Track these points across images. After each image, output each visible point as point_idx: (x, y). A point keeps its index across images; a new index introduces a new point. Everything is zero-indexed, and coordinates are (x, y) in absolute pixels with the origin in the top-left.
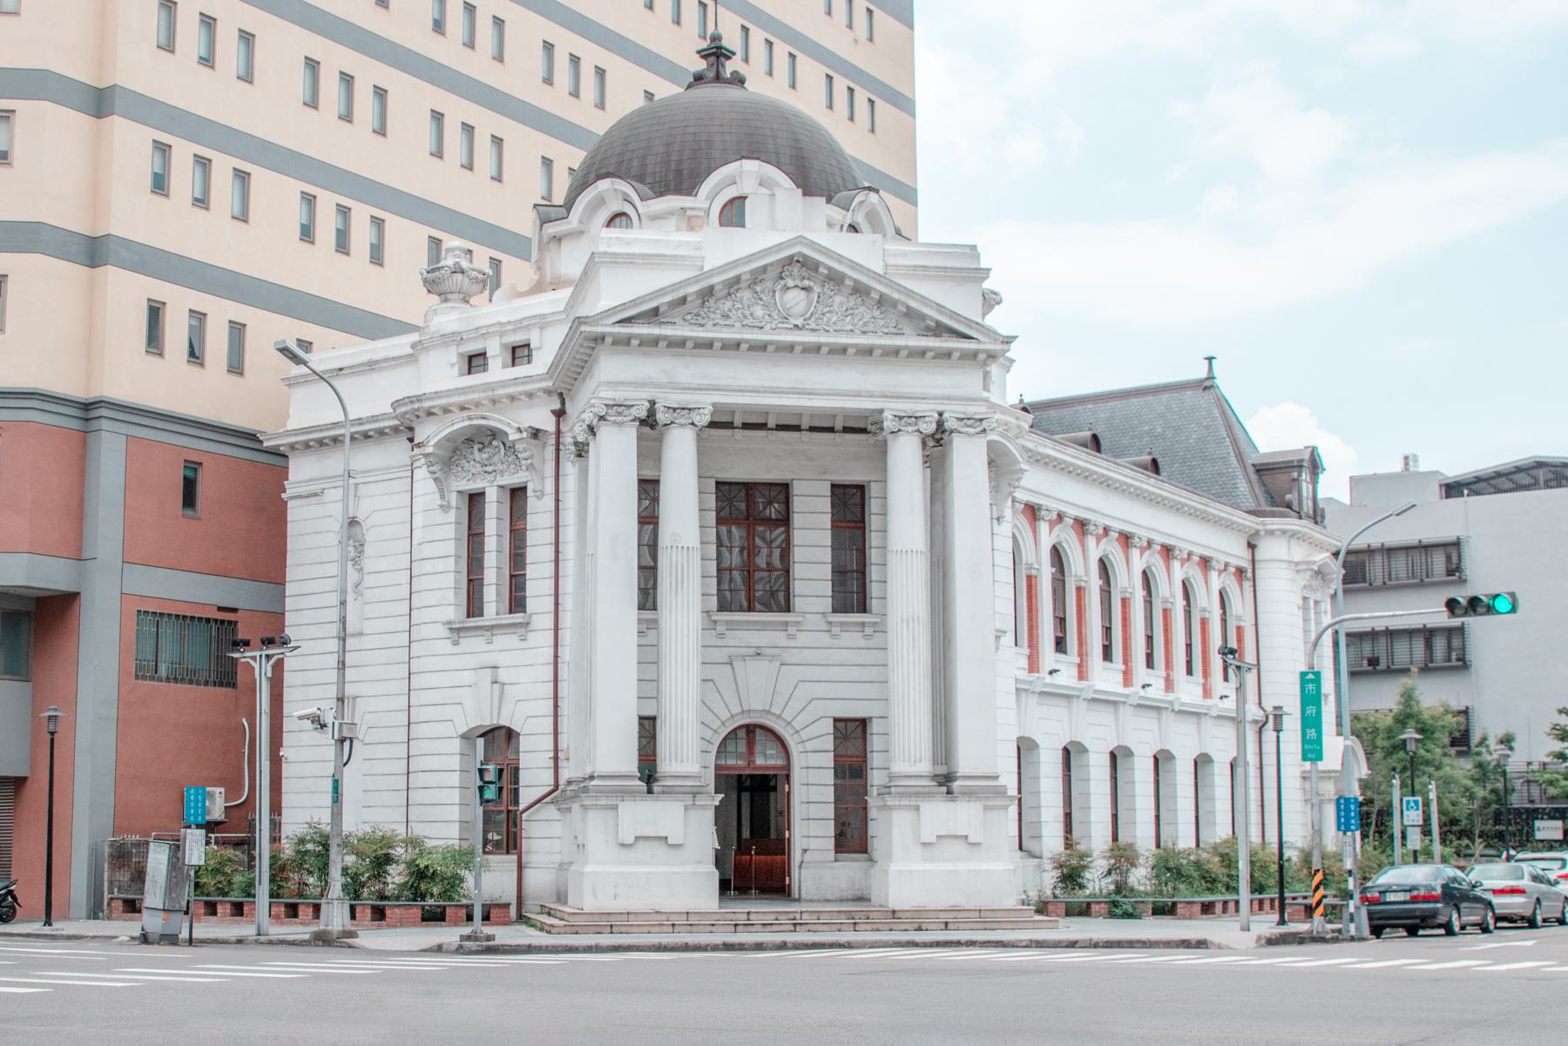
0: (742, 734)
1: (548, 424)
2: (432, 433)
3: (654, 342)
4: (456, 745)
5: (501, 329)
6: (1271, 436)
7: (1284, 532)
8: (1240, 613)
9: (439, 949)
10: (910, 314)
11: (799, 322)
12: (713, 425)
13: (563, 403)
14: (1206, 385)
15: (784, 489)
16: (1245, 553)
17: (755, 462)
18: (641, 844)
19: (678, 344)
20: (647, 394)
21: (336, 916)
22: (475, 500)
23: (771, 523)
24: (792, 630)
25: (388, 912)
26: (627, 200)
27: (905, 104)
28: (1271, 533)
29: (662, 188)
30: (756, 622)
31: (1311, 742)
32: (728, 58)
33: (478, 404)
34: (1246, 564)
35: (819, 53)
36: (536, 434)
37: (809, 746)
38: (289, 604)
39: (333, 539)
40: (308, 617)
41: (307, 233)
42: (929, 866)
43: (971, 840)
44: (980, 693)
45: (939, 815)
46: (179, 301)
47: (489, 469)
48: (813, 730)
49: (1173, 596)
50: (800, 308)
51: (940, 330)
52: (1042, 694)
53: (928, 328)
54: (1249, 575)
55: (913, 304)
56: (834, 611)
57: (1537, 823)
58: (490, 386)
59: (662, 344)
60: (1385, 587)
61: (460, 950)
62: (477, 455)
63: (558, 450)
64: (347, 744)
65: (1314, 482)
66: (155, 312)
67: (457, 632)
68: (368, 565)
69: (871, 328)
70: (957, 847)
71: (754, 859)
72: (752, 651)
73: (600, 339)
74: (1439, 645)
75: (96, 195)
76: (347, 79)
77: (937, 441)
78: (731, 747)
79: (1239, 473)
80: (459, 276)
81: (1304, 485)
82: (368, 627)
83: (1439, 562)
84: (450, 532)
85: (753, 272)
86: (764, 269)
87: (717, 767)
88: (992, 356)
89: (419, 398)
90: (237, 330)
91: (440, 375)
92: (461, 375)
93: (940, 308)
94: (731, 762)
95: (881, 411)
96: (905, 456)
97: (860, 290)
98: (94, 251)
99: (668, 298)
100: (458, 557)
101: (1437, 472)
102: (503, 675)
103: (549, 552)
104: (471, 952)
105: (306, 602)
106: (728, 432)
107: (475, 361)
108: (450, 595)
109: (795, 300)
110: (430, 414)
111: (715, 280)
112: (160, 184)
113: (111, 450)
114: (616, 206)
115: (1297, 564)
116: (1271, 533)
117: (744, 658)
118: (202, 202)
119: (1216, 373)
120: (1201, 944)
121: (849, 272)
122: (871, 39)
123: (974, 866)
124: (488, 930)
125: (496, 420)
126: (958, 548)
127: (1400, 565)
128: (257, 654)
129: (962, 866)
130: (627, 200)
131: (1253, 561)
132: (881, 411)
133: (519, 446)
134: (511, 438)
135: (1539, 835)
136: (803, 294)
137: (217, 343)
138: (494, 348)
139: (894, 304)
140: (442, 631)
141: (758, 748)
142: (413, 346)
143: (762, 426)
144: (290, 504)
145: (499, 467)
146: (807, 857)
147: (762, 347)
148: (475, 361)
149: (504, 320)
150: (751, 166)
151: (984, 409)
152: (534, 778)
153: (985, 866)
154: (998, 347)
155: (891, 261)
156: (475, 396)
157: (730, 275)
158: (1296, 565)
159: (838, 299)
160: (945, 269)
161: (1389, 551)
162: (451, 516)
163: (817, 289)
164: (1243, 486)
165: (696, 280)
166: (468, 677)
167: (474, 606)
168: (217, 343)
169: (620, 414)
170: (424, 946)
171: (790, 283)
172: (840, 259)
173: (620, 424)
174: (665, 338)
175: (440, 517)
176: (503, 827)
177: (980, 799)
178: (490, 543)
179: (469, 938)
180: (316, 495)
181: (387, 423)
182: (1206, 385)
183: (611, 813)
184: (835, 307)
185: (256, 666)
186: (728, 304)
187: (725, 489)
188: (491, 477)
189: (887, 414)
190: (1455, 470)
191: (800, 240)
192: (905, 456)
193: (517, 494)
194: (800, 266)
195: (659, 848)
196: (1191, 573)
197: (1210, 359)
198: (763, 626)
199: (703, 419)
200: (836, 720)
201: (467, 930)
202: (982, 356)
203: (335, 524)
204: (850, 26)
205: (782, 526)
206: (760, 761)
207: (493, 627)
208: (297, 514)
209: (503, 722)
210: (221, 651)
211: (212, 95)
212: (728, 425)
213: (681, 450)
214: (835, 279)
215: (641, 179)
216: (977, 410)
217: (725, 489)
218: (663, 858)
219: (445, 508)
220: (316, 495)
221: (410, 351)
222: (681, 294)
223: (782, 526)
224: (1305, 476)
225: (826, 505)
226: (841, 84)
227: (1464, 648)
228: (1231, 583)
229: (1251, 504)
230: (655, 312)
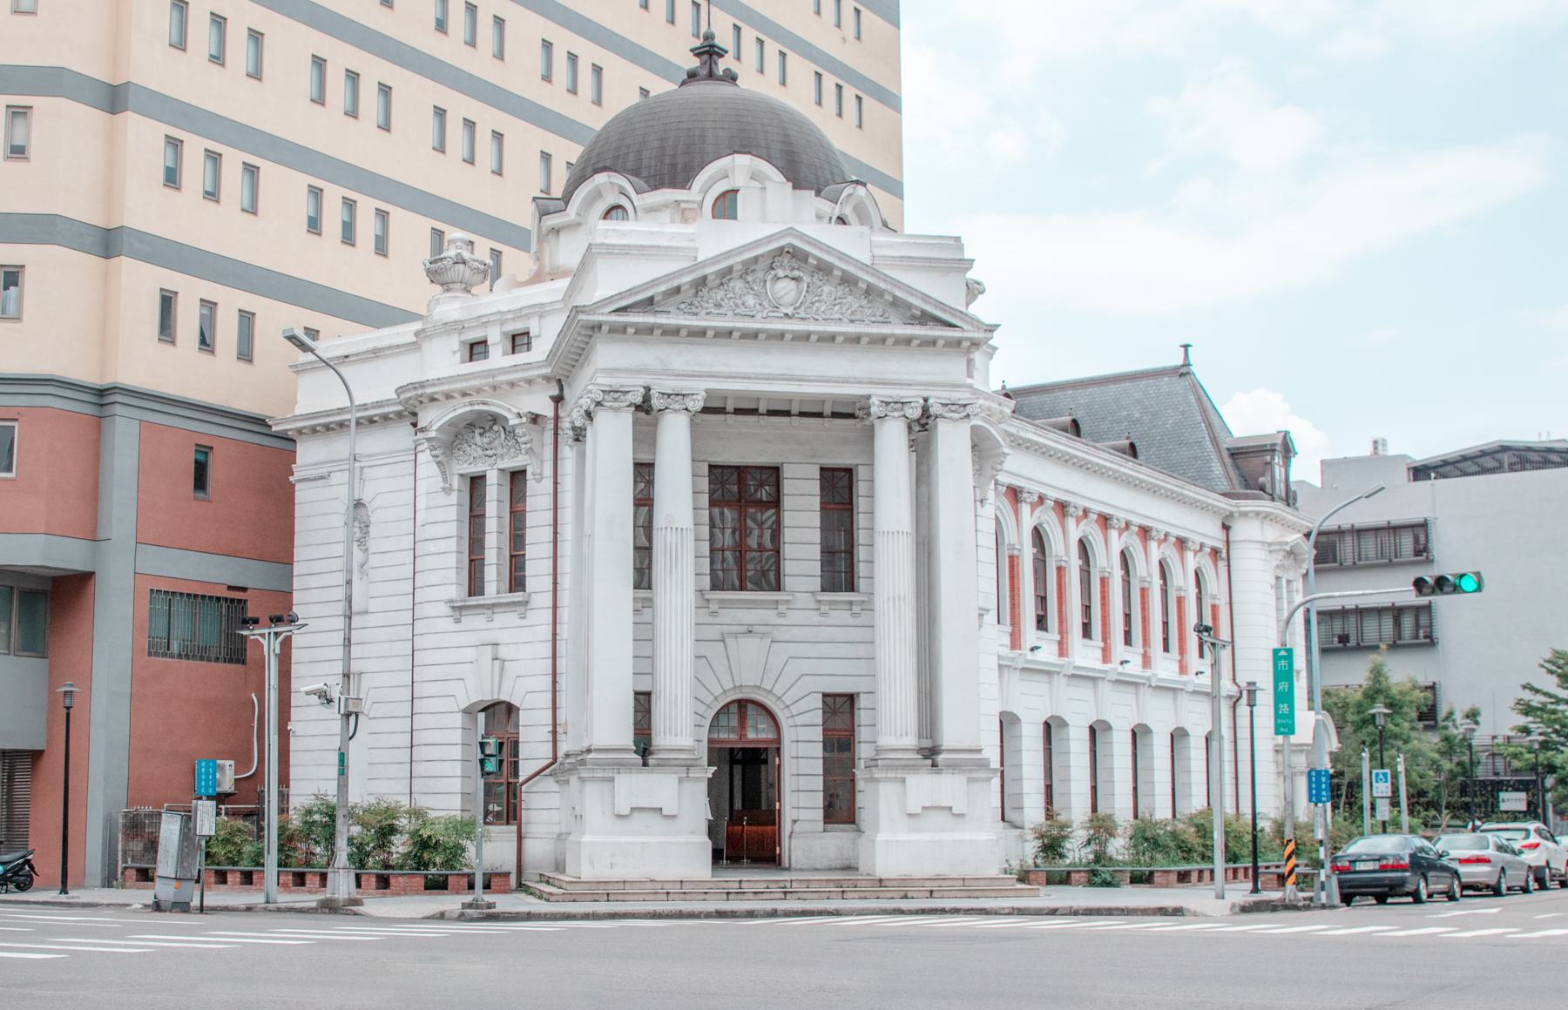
0: (734, 708)
1: (547, 409)
2: (435, 418)
3: (650, 330)
4: (458, 720)
5: (501, 317)
6: (1245, 419)
7: (1257, 514)
8: (1215, 592)
9: (441, 916)
10: (896, 303)
11: (790, 311)
12: (706, 410)
13: (561, 389)
14: (1183, 372)
15: (775, 471)
16: (1221, 535)
17: (746, 446)
18: (636, 815)
19: (672, 332)
20: (642, 380)
21: (342, 884)
24: (782, 608)
25: (392, 881)
26: (623, 193)
27: (891, 100)
28: (1245, 515)
29: (657, 182)
30: (754, 601)
31: (1283, 716)
32: (721, 56)
33: (479, 390)
34: (1221, 545)
35: (809, 52)
36: (535, 419)
37: (799, 720)
39: (338, 521)
40: (315, 596)
41: (314, 225)
42: (914, 837)
43: (955, 811)
45: (924, 787)
47: (490, 453)
48: (803, 706)
49: (1150, 575)
50: (791, 296)
51: (925, 318)
53: (914, 317)
54: (1224, 555)
55: (899, 293)
56: (823, 590)
57: (1502, 795)
58: (503, 371)
59: (657, 332)
60: (1354, 567)
61: (461, 918)
62: (478, 439)
63: (556, 434)
64: (352, 719)
65: (1287, 465)
66: (167, 302)
67: (459, 610)
68: (373, 545)
69: (858, 316)
70: (943, 818)
72: (744, 629)
73: (596, 327)
74: (1407, 623)
75: (110, 190)
76: (353, 77)
77: (922, 426)
78: (723, 721)
79: (1214, 456)
80: (461, 267)
82: (373, 605)
83: (1407, 543)
84: (452, 513)
85: (745, 263)
86: (756, 259)
87: (710, 741)
88: (975, 344)
89: (422, 385)
90: (247, 318)
91: (442, 362)
92: (463, 362)
93: (925, 297)
94: (723, 736)
95: (868, 397)
96: (892, 441)
97: (848, 280)
98: (109, 242)
99: (663, 288)
100: (460, 538)
102: (503, 652)
105: (313, 582)
106: (786, 419)
107: (476, 349)
108: (452, 574)
109: (785, 289)
110: (433, 399)
111: (709, 270)
112: (172, 178)
113: (125, 432)
114: (612, 199)
115: (1270, 544)
116: (1245, 515)
117: (736, 635)
118: (213, 195)
119: (1192, 359)
120: (1177, 912)
121: (837, 263)
122: (858, 38)
123: (958, 836)
124: (489, 898)
125: (497, 406)
126: (945, 530)
128: (266, 631)
129: (947, 837)
130: (623, 193)
131: (1228, 542)
132: (868, 397)
133: (519, 431)
134: (511, 423)
135: (1503, 807)
137: (227, 331)
138: (495, 336)
140: (444, 609)
141: (750, 722)
142: (417, 334)
143: (753, 412)
144: (298, 486)
145: (500, 451)
146: (797, 827)
147: (753, 335)
148: (476, 349)
149: (504, 309)
150: (743, 160)
151: (967, 395)
152: (533, 751)
153: (968, 836)
154: (982, 335)
157: (723, 265)
158: (1269, 546)
159: (827, 289)
161: (1359, 532)
162: (454, 498)
163: (806, 279)
164: (1217, 469)
165: (690, 270)
166: (469, 654)
167: (475, 585)
168: (227, 331)
169: (616, 400)
170: (427, 914)
171: (781, 273)
172: (829, 250)
173: (616, 410)
174: (660, 326)
175: (442, 499)
176: (503, 798)
177: (963, 772)
179: (470, 906)
180: (322, 478)
181: (391, 409)
182: (1183, 372)
184: (824, 297)
185: (265, 643)
186: (721, 294)
188: (491, 460)
189: (874, 400)
190: (1423, 453)
191: (790, 232)
192: (892, 441)
193: (517, 477)
194: (791, 257)
197: (1186, 347)
198: (755, 604)
199: (696, 404)
201: (468, 898)
202: (966, 344)
203: (341, 506)
204: (838, 26)
205: (767, 510)
206: (751, 735)
207: (493, 605)
208: (304, 496)
210: (231, 628)
211: (223, 92)
212: (721, 411)
213: (675, 435)
214: (824, 269)
215: (636, 172)
216: (962, 396)
218: (653, 830)
219: (447, 490)
220: (322, 478)
222: (675, 283)
223: (767, 510)
224: (1278, 459)
225: (815, 487)
226: (829, 81)
227: (1431, 626)
228: (1206, 563)
229: (1225, 487)
230: (650, 301)
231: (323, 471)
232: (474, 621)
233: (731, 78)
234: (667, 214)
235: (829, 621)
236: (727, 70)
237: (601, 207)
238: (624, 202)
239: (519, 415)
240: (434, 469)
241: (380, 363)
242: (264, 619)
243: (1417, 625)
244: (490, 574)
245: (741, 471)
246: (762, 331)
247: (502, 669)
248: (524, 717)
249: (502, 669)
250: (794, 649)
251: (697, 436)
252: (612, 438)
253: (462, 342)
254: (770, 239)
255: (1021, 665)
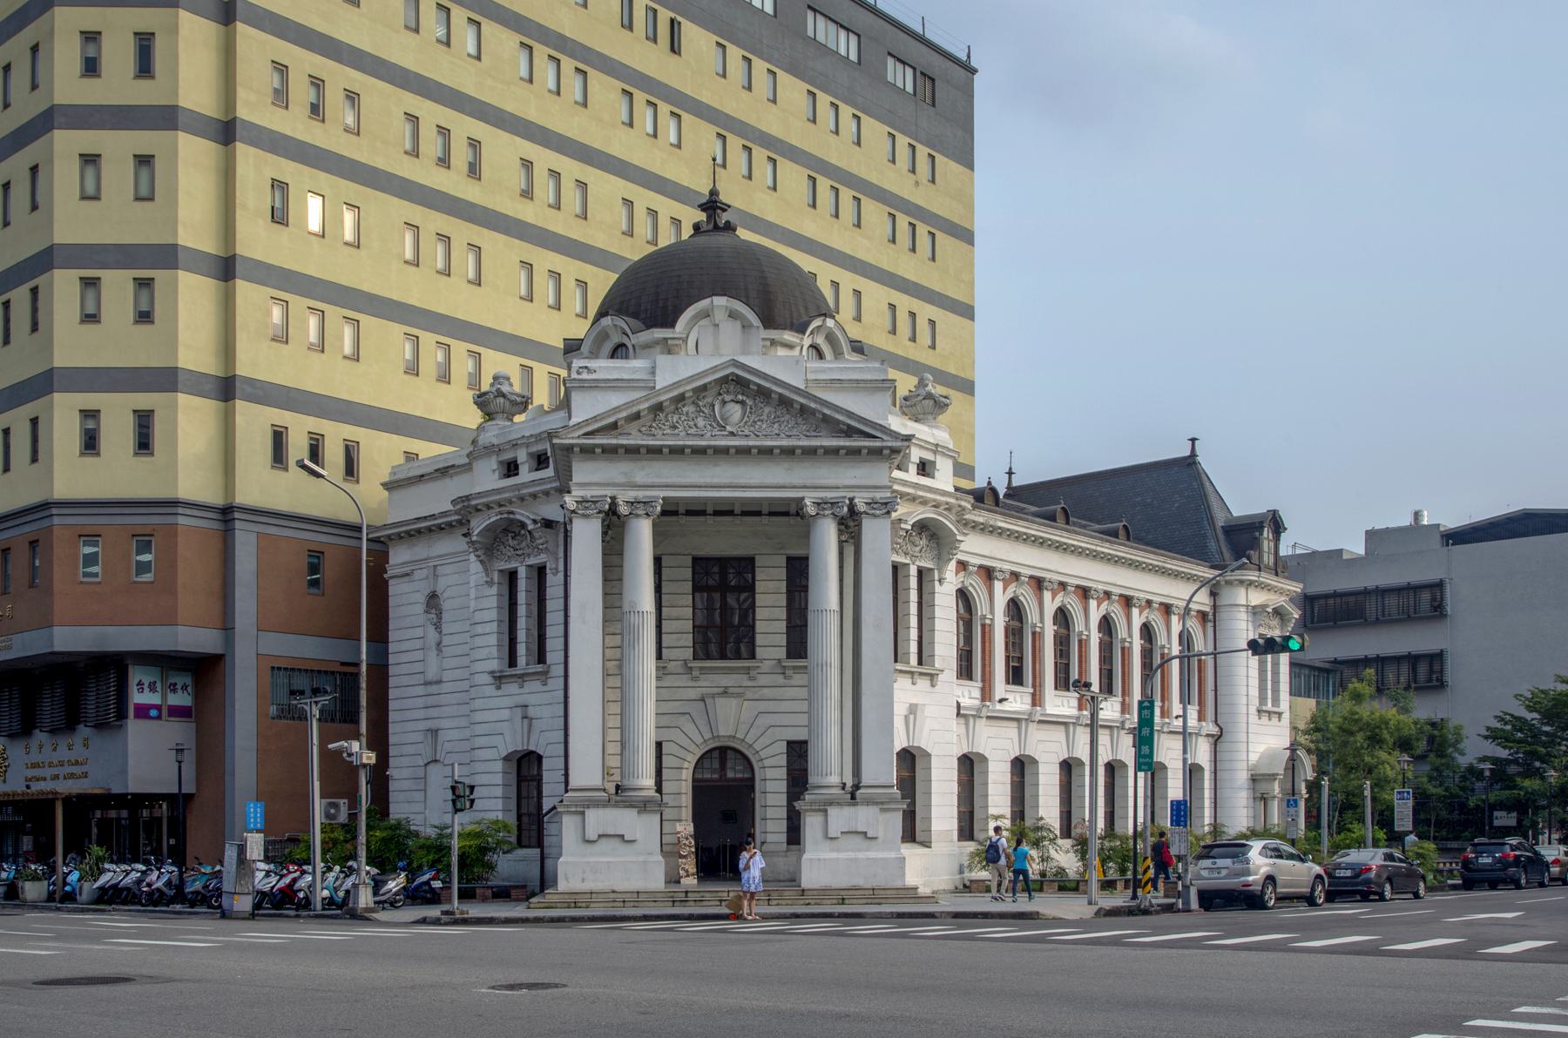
0: (716, 754)
2: (478, 525)
4: (499, 766)
5: (525, 442)
9: (423, 921)
10: (826, 419)
12: (664, 513)
14: (1190, 462)
17: (722, 541)
18: (603, 840)
19: (632, 451)
20: (609, 492)
22: (512, 576)
23: (739, 589)
24: (753, 673)
27: (966, 236)
28: (1229, 583)
29: (651, 323)
31: (1145, 756)
35: (881, 195)
38: (392, 659)
39: (420, 608)
40: (404, 669)
42: (834, 855)
44: (937, 723)
46: (299, 427)
51: (850, 432)
52: (1040, 722)
57: (1496, 814)
60: (1377, 622)
61: (436, 922)
62: (511, 542)
65: (1277, 539)
67: (499, 679)
68: (446, 629)
71: (718, 855)
74: (1422, 669)
77: (850, 524)
78: (707, 763)
81: (1265, 543)
84: (493, 602)
87: (694, 780)
89: (468, 498)
91: (486, 478)
93: (850, 414)
96: (827, 536)
97: (784, 402)
99: (624, 414)
100: (500, 621)
101: (1438, 526)
102: (531, 712)
103: (560, 617)
104: (446, 924)
105: (404, 658)
106: (757, 519)
107: (511, 468)
108: (494, 651)
109: (735, 411)
111: (662, 398)
113: (246, 541)
114: (616, 339)
119: (1198, 451)
121: (774, 388)
122: (933, 181)
123: (872, 855)
127: (1392, 601)
129: (861, 855)
131: (1215, 607)
133: (536, 535)
136: (737, 407)
137: (334, 454)
138: (522, 456)
139: (813, 412)
140: (487, 679)
141: (729, 764)
143: (730, 513)
144: (391, 582)
145: (527, 551)
148: (511, 468)
150: (720, 301)
153: (880, 855)
154: (899, 444)
155: (811, 376)
156: (507, 495)
157: (675, 393)
159: (767, 410)
160: (857, 381)
161: (1382, 592)
162: (494, 590)
163: (749, 402)
165: (646, 398)
166: (506, 714)
167: (512, 662)
168: (334, 454)
174: (622, 446)
178: (522, 610)
182: (1190, 462)
183: (578, 818)
185: (307, 708)
186: (676, 418)
187: (701, 565)
189: (808, 502)
192: (827, 536)
193: (541, 571)
194: (737, 384)
195: (616, 843)
196: (1151, 617)
197: (1193, 440)
198: (731, 670)
200: (789, 743)
202: (886, 452)
203: (421, 598)
204: (913, 171)
205: (731, 592)
206: (730, 774)
207: (521, 676)
209: (532, 748)
210: (353, 693)
212: (675, 513)
213: (642, 535)
214: (763, 394)
215: (635, 315)
217: (701, 565)
218: (616, 854)
219: (490, 583)
221: (467, 460)
222: (635, 409)
223: (731, 592)
224: (1267, 533)
227: (1442, 671)
228: (1193, 624)
230: (614, 426)
231: (406, 569)
232: (511, 688)
233: (729, 227)
234: (658, 348)
235: (793, 682)
236: (728, 223)
237: (608, 347)
238: (625, 340)
239: (535, 521)
240: (479, 567)
241: (447, 481)
242: (308, 692)
243: (1431, 671)
244: (521, 649)
245: (723, 562)
246: (709, 447)
247: (530, 726)
248: (546, 764)
249: (530, 726)
250: (762, 706)
251: (659, 535)
252: (586, 538)
253: (501, 463)
254: (714, 369)
255: (1038, 718)
